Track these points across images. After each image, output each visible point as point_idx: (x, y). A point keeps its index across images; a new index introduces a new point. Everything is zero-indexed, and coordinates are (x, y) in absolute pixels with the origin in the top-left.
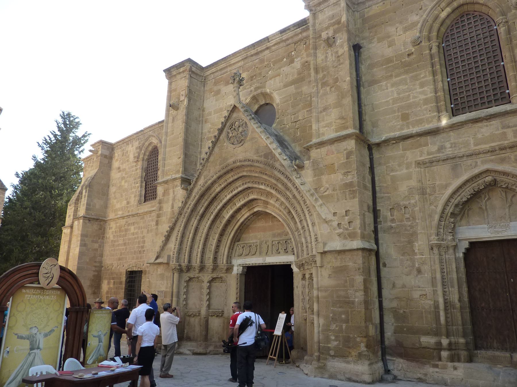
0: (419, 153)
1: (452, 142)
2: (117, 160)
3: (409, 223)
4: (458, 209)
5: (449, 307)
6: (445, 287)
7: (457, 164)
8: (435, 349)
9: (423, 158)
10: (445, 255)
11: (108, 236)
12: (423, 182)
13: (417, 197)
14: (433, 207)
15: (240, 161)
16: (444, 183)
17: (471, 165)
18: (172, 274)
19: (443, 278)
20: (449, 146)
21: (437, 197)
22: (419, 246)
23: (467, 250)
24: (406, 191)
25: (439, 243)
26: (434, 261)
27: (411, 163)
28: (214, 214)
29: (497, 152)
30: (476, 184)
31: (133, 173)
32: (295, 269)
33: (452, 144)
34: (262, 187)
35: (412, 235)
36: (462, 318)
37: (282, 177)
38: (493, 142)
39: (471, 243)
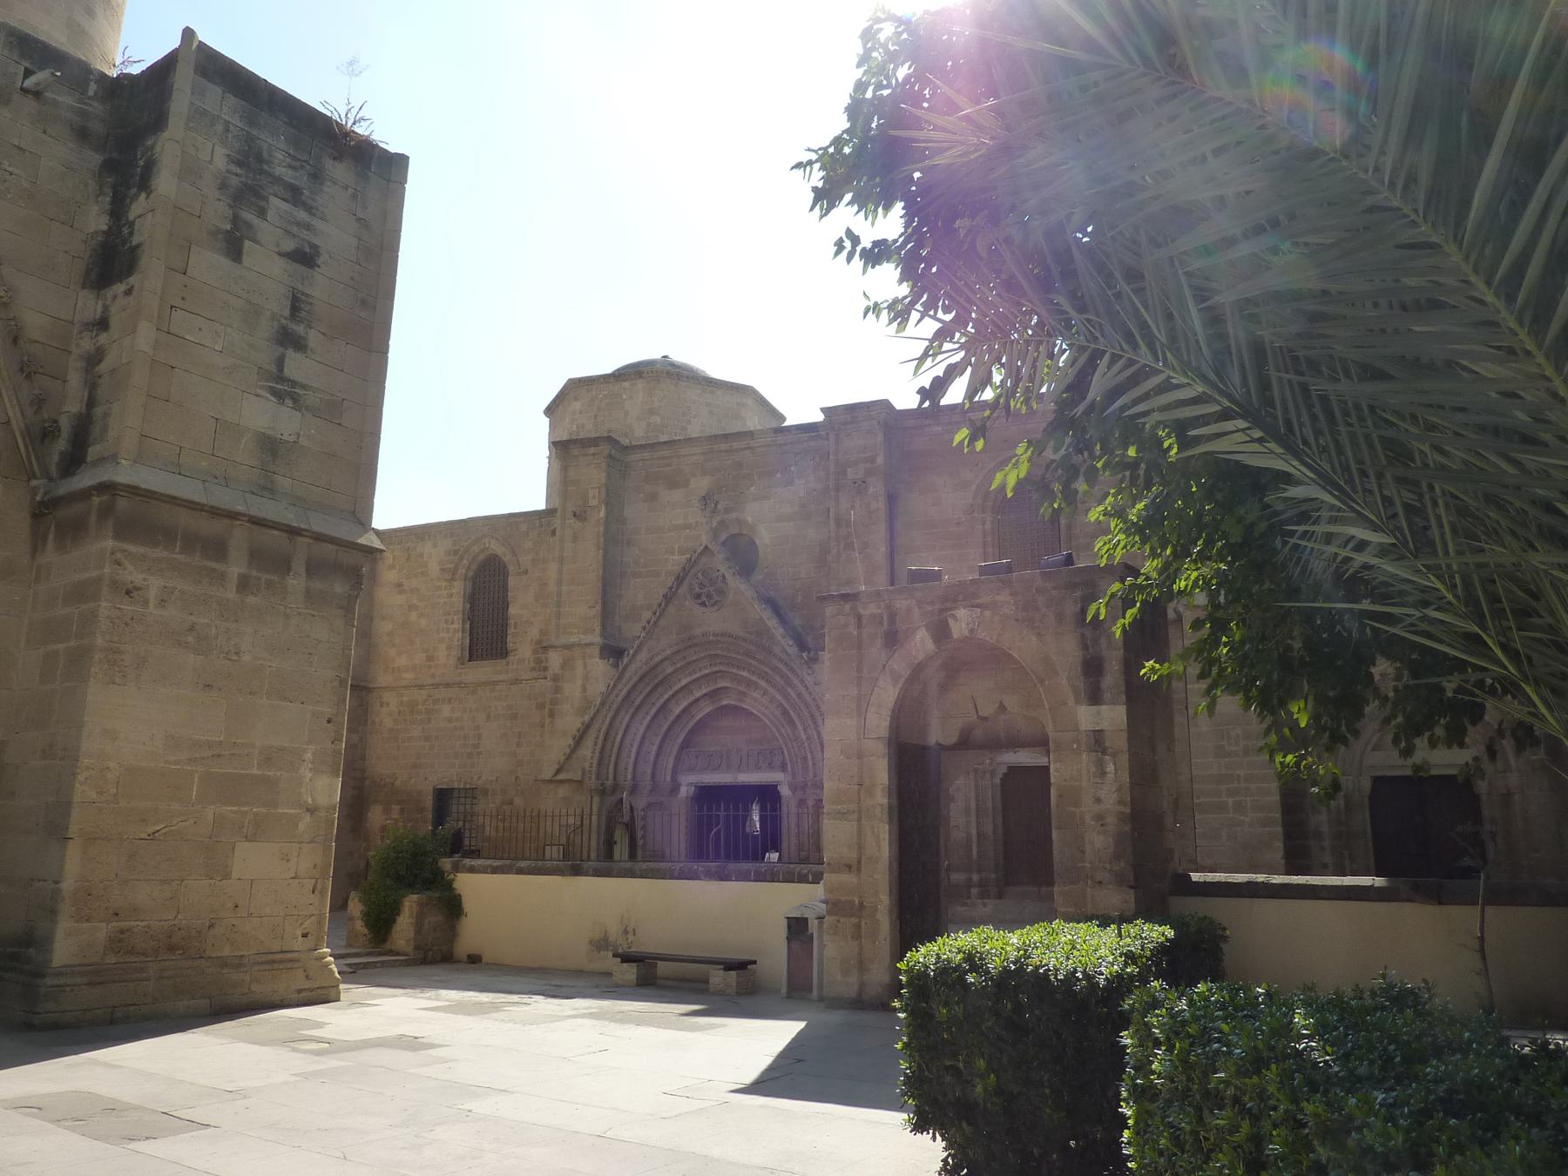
2: (392, 567)
11: (377, 720)
15: (714, 634)
18: (589, 798)
23: (1004, 774)
28: (658, 705)
31: (442, 601)
32: (785, 791)
34: (745, 674)
37: (781, 666)
39: (1010, 768)
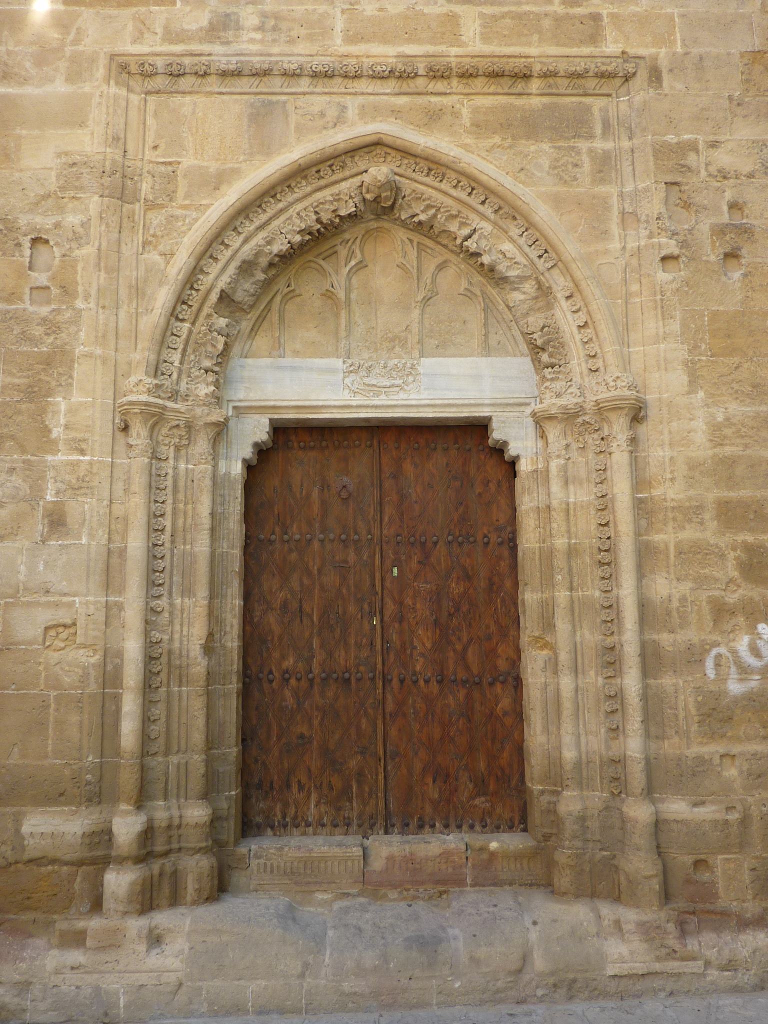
0: (130, 27)
1: (268, 8)
3: (44, 310)
4: (248, 285)
5: (163, 675)
6: (155, 591)
7: (271, 103)
8: (80, 863)
9: (145, 49)
10: (176, 459)
12: (130, 147)
13: (94, 203)
14: (154, 257)
16: (214, 167)
17: (322, 114)
19: (153, 553)
20: (255, 21)
21: (177, 218)
22: (71, 411)
23: (262, 452)
24: (53, 173)
25: (156, 405)
26: (128, 481)
27: (93, 60)
29: (421, 82)
30: (326, 194)
33: (264, 15)
35: (48, 361)
36: (208, 717)
38: (409, 41)
